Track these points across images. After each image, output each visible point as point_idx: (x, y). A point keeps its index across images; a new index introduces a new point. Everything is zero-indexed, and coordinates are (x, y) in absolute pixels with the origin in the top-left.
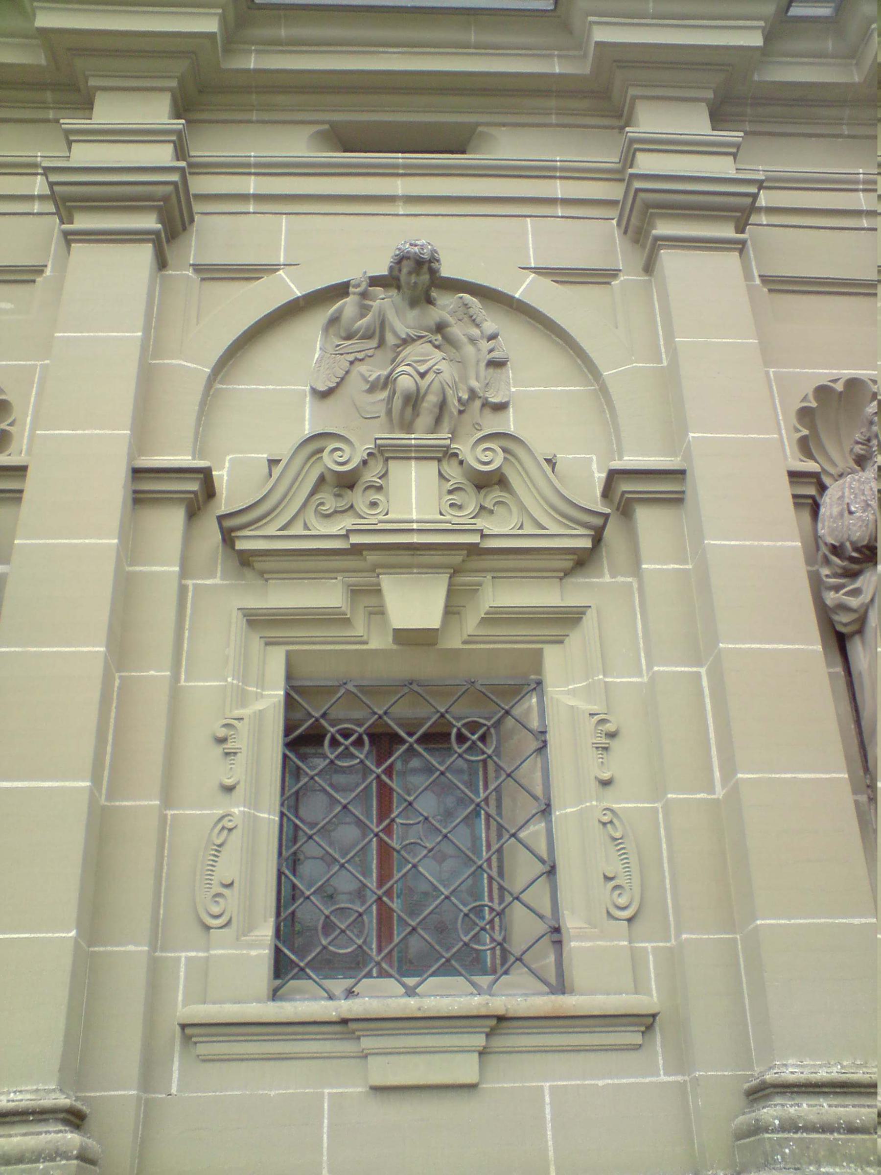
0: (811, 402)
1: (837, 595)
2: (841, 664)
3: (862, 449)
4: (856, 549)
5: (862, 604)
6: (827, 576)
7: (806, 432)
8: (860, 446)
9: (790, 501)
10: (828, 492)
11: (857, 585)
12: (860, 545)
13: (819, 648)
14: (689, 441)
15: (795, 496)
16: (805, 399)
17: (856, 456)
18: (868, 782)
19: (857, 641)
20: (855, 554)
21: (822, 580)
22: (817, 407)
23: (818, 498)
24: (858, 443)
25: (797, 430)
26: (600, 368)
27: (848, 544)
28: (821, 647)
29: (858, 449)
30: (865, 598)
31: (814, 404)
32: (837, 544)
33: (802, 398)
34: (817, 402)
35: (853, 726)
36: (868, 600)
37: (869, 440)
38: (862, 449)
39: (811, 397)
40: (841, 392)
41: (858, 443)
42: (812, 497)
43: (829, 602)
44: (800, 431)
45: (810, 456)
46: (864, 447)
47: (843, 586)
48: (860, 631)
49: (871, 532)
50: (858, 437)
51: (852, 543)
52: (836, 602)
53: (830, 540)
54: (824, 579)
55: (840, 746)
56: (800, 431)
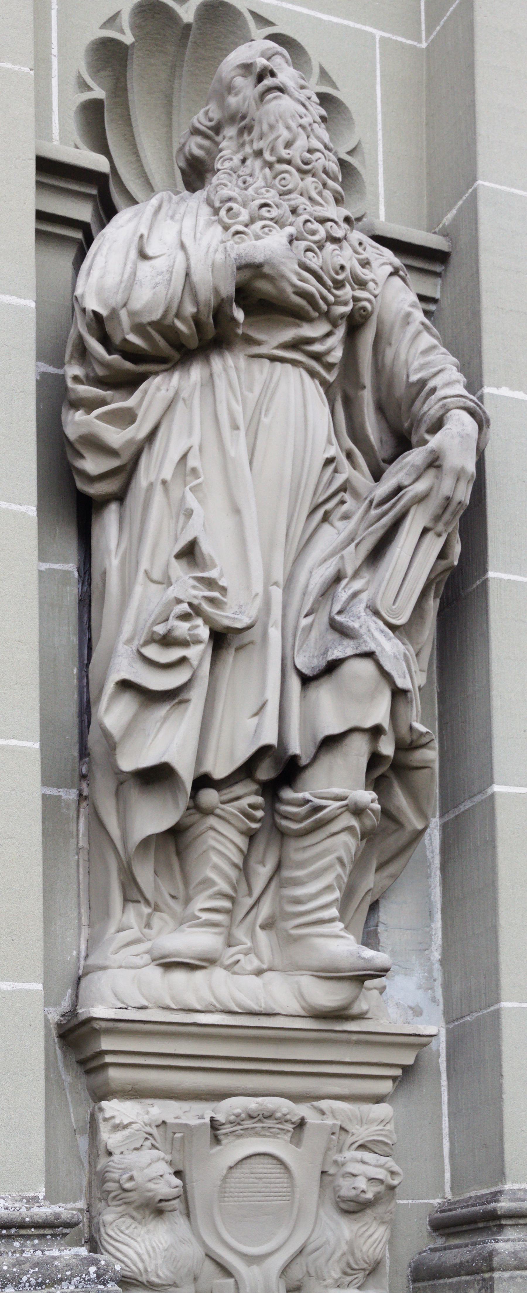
0: (122, 32)
1: (88, 416)
2: (77, 562)
3: (201, 147)
4: (139, 329)
5: (130, 442)
6: (76, 379)
7: (99, 93)
8: (199, 139)
9: (31, 224)
10: (117, 220)
11: (131, 402)
12: (146, 319)
13: (32, 511)
14: (442, 816)
15: (41, 216)
16: (112, 21)
17: (187, 160)
18: (84, 770)
19: (112, 513)
20: (133, 338)
21: (66, 388)
22: (133, 44)
23: (94, 228)
24: (196, 132)
25: (84, 86)
26: (38, 757)
27: (123, 314)
28: (35, 509)
29: (195, 147)
30: (139, 431)
31: (128, 38)
32: (104, 312)
33: (105, 19)
34: (134, 36)
35: (75, 671)
36: (143, 433)
37: (217, 129)
38: (201, 147)
39: (125, 20)
40: (188, 26)
41: (196, 132)
42: (84, 227)
43: (72, 433)
44: (90, 89)
45: (103, 148)
46: (206, 143)
47: (103, 402)
48: (120, 497)
49: (171, 300)
50: (200, 119)
51: (132, 314)
52: (84, 431)
53: (92, 304)
54: (70, 383)
55: (34, 694)
56: (90, 89)
